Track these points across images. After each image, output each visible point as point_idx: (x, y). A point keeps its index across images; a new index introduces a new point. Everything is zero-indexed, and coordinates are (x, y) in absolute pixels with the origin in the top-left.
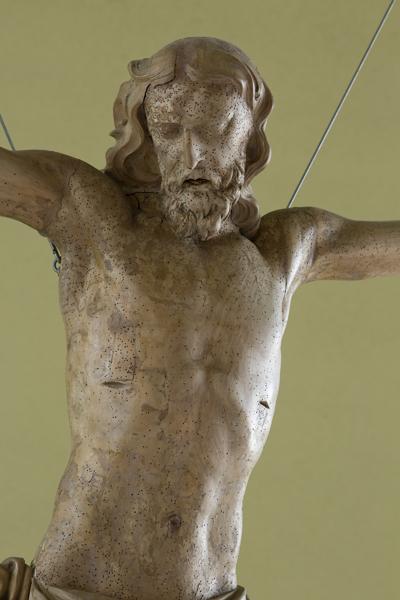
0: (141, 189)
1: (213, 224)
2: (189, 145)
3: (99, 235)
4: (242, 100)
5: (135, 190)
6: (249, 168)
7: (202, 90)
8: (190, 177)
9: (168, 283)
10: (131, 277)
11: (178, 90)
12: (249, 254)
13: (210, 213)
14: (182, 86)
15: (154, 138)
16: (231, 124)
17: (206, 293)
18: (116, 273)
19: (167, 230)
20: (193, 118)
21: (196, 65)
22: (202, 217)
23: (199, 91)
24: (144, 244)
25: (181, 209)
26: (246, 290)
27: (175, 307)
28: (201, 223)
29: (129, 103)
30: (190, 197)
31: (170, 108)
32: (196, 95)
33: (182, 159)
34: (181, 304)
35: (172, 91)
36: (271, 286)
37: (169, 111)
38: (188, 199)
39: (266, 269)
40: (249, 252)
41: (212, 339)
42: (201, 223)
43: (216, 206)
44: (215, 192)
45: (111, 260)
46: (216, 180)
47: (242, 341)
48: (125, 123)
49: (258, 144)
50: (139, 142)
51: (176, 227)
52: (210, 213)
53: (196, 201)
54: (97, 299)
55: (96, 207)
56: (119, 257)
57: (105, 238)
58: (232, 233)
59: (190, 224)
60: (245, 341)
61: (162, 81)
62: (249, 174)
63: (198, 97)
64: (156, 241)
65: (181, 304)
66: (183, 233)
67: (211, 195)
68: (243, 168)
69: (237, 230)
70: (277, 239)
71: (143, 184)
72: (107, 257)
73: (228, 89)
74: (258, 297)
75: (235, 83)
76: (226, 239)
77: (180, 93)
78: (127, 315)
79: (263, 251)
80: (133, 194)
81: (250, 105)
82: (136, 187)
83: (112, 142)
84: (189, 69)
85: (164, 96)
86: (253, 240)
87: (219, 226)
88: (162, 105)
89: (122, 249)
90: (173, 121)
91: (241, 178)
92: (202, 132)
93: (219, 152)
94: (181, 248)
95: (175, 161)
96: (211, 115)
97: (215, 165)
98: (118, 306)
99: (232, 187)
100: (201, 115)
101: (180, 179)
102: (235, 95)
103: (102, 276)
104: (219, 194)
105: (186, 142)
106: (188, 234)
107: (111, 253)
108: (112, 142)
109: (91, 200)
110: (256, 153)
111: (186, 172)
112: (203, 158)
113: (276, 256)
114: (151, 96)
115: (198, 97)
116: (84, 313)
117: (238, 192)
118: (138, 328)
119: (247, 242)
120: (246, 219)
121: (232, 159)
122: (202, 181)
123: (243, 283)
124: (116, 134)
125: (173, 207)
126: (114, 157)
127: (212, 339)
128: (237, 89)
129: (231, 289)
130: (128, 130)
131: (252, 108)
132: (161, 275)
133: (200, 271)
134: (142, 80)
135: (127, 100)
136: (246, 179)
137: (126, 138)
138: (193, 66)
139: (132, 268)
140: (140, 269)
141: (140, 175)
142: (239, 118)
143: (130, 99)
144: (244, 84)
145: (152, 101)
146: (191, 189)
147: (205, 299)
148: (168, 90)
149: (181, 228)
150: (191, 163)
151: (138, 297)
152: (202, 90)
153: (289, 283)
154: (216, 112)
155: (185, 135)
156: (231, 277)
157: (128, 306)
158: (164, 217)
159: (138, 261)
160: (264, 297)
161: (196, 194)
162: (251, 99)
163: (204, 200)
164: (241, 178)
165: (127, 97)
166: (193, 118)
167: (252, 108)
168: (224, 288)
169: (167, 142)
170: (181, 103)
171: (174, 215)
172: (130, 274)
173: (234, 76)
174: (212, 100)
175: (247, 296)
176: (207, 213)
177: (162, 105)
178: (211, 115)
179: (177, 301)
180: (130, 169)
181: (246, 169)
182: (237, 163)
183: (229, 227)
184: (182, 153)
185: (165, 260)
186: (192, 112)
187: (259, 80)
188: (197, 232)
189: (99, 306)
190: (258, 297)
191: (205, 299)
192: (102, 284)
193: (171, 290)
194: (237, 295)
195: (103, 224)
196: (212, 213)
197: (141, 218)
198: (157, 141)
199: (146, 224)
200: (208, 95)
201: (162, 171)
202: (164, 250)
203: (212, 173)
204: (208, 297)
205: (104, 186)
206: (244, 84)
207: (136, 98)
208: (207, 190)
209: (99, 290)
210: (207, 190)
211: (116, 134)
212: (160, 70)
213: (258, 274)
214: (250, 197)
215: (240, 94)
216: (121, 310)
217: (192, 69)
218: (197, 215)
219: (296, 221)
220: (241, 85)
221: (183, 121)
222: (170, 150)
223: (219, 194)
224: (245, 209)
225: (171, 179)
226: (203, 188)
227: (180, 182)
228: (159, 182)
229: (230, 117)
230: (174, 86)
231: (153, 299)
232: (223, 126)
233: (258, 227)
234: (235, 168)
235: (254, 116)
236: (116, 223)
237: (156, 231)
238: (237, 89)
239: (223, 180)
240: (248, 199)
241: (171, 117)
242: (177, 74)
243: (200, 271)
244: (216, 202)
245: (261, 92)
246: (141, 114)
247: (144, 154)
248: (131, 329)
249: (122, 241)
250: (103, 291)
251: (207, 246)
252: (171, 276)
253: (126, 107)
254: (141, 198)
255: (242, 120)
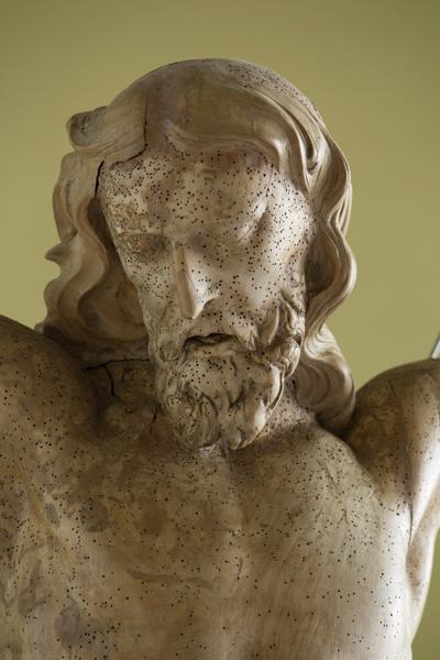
0: (119, 355)
1: (250, 418)
2: (183, 274)
3: (32, 456)
4: (281, 178)
5: (106, 357)
6: (311, 307)
7: (199, 166)
8: (196, 332)
9: (166, 541)
10: (96, 535)
11: (153, 169)
12: (330, 465)
13: (242, 397)
14: (162, 162)
15: (122, 259)
16: (263, 226)
17: (242, 554)
18: (67, 529)
19: (164, 433)
20: (185, 222)
21: (185, 123)
22: (227, 404)
23: (192, 170)
24: (119, 467)
25: (187, 395)
26: (325, 537)
27: (180, 587)
28: (225, 418)
29: (72, 196)
30: (202, 368)
31: (142, 207)
32: (187, 177)
33: (176, 301)
34: (194, 580)
35: (142, 173)
36: (378, 525)
37: (139, 212)
38: (196, 372)
39: (368, 493)
40: (333, 459)
41: (259, 643)
42: (225, 418)
43: (253, 383)
44: (248, 356)
45: (56, 504)
46: (247, 331)
47: (319, 641)
48: (74, 233)
49: (328, 255)
50: (99, 270)
51: (181, 429)
52: (242, 397)
53: (213, 376)
54: (35, 580)
55: (22, 403)
56: (70, 498)
57: (42, 463)
58: (298, 428)
59: (205, 421)
60: (325, 641)
61: (125, 154)
62: (314, 314)
63: (192, 182)
64: (142, 458)
65: (194, 580)
66: (195, 438)
67: (240, 361)
68: (301, 306)
69: (308, 419)
70: (389, 428)
71: (121, 343)
72: (48, 499)
73: (249, 162)
74: (347, 552)
75: (262, 147)
76: (289, 441)
77: (159, 176)
78: (91, 609)
79: (363, 457)
80: (104, 365)
81: (299, 184)
82: (109, 350)
83: (53, 271)
84: (172, 130)
85: (128, 182)
86: (343, 434)
87: (261, 419)
88: (127, 200)
89: (74, 481)
90: (150, 230)
91: (298, 323)
92: (207, 245)
93: (245, 282)
94: (193, 469)
95: (164, 303)
96: (220, 214)
97: (242, 307)
98: (74, 594)
99: (281, 341)
100: (200, 214)
101: (178, 337)
102: (265, 169)
103: (43, 536)
104: (256, 358)
105: (177, 267)
106: (203, 441)
107: (54, 492)
108: (53, 271)
109: (12, 389)
110: (322, 271)
111: (186, 325)
112: (215, 295)
113: (388, 462)
114: (106, 183)
115: (192, 182)
116: (14, 610)
117: (295, 351)
118: (112, 634)
119: (328, 441)
120: (325, 395)
121: (275, 290)
122: (220, 337)
123: (318, 526)
124: (57, 255)
125: (172, 390)
126: (57, 297)
127: (259, 643)
128: (267, 156)
129: (293, 540)
130: (78, 245)
131: (304, 190)
132: (152, 526)
133: (231, 511)
134: (91, 155)
135: (68, 192)
136: (308, 324)
137: (76, 262)
138: (178, 122)
139: (95, 518)
140: (111, 519)
141: (113, 328)
142: (278, 213)
143: (72, 188)
144: (280, 146)
145: (109, 194)
146: (200, 354)
147: (240, 566)
148: (136, 172)
149: (189, 431)
150: (191, 308)
151: (108, 574)
152: (199, 166)
153: (418, 517)
154: (229, 207)
155: (175, 254)
156: (292, 516)
157: (92, 593)
158: (159, 409)
159: (106, 503)
160: (362, 549)
161: (213, 364)
162: (301, 175)
163: (228, 373)
164: (298, 323)
165: (68, 185)
166: (185, 222)
167: (304, 190)
168: (280, 531)
169: (145, 269)
170: (160, 194)
171: (174, 406)
172: (92, 530)
173: (258, 135)
174: (219, 185)
175: (325, 551)
176: (235, 397)
177: (127, 201)
178: (220, 214)
179: (184, 574)
180: (92, 320)
181: (307, 305)
182: (286, 297)
183: (292, 415)
184: (174, 289)
185: (159, 496)
186: (185, 210)
187: (312, 136)
188: (220, 435)
189: (39, 595)
190: (347, 552)
191: (240, 566)
192: (44, 552)
193: (173, 554)
194: (305, 550)
195: (38, 434)
196: (245, 398)
197: (114, 414)
198: (129, 267)
199: (123, 426)
200: (211, 175)
201: (146, 320)
202: (159, 474)
203: (236, 319)
204: (246, 562)
205: (36, 359)
206: (280, 146)
207: (82, 190)
208: (230, 353)
209: (40, 561)
210: (230, 353)
211: (57, 255)
212: (119, 133)
213: (350, 504)
214: (328, 353)
215: (275, 165)
216: (79, 600)
217: (177, 129)
218: (218, 403)
219: (427, 388)
220: (274, 150)
221: (169, 229)
222: (153, 280)
223: (256, 358)
224: (316, 383)
225: (163, 337)
226: (223, 351)
227: (178, 343)
228: (146, 339)
229: (259, 213)
230: (146, 163)
231: (137, 575)
232: (246, 231)
233: (351, 408)
234: (284, 307)
235: (311, 202)
236: (61, 432)
237: (142, 438)
238: (267, 156)
239: (260, 331)
240: (324, 359)
241: (145, 223)
242: (149, 140)
243: (231, 511)
244: (250, 375)
245: (322, 155)
246: (96, 215)
247: (114, 291)
248: (99, 636)
249: (76, 464)
250: (45, 565)
251: (247, 459)
252: (173, 525)
253: (68, 205)
254: (118, 373)
255: (291, 222)
